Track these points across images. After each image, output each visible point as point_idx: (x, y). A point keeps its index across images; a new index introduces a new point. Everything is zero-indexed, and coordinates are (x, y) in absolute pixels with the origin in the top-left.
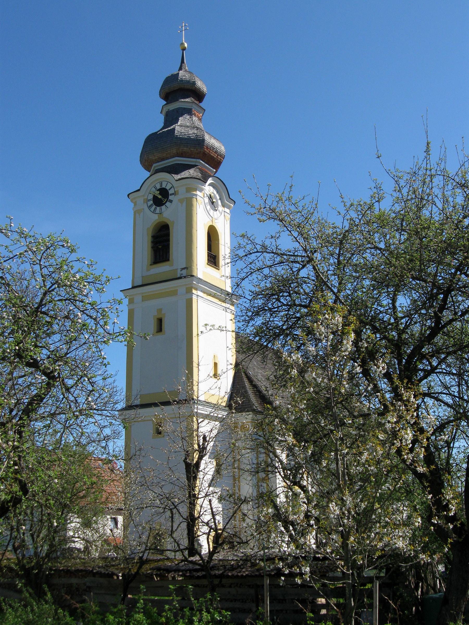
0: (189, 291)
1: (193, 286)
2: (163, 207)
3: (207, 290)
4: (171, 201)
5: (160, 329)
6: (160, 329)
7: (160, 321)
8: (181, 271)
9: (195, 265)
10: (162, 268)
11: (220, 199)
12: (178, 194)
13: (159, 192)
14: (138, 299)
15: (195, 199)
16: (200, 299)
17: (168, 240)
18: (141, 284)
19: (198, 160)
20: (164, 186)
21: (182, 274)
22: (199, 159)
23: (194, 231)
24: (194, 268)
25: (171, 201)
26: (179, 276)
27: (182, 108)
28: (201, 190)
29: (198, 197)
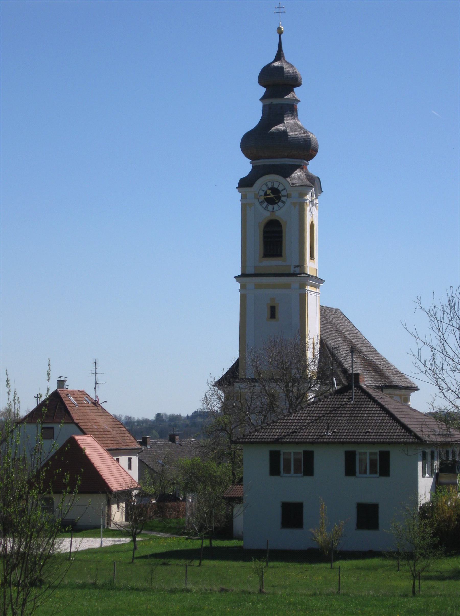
0: (302, 287)
2: (276, 206)
8: (294, 268)
15: (306, 203)
17: (281, 237)
18: (253, 272)
20: (276, 186)
21: (295, 271)
25: (284, 202)
26: (292, 272)
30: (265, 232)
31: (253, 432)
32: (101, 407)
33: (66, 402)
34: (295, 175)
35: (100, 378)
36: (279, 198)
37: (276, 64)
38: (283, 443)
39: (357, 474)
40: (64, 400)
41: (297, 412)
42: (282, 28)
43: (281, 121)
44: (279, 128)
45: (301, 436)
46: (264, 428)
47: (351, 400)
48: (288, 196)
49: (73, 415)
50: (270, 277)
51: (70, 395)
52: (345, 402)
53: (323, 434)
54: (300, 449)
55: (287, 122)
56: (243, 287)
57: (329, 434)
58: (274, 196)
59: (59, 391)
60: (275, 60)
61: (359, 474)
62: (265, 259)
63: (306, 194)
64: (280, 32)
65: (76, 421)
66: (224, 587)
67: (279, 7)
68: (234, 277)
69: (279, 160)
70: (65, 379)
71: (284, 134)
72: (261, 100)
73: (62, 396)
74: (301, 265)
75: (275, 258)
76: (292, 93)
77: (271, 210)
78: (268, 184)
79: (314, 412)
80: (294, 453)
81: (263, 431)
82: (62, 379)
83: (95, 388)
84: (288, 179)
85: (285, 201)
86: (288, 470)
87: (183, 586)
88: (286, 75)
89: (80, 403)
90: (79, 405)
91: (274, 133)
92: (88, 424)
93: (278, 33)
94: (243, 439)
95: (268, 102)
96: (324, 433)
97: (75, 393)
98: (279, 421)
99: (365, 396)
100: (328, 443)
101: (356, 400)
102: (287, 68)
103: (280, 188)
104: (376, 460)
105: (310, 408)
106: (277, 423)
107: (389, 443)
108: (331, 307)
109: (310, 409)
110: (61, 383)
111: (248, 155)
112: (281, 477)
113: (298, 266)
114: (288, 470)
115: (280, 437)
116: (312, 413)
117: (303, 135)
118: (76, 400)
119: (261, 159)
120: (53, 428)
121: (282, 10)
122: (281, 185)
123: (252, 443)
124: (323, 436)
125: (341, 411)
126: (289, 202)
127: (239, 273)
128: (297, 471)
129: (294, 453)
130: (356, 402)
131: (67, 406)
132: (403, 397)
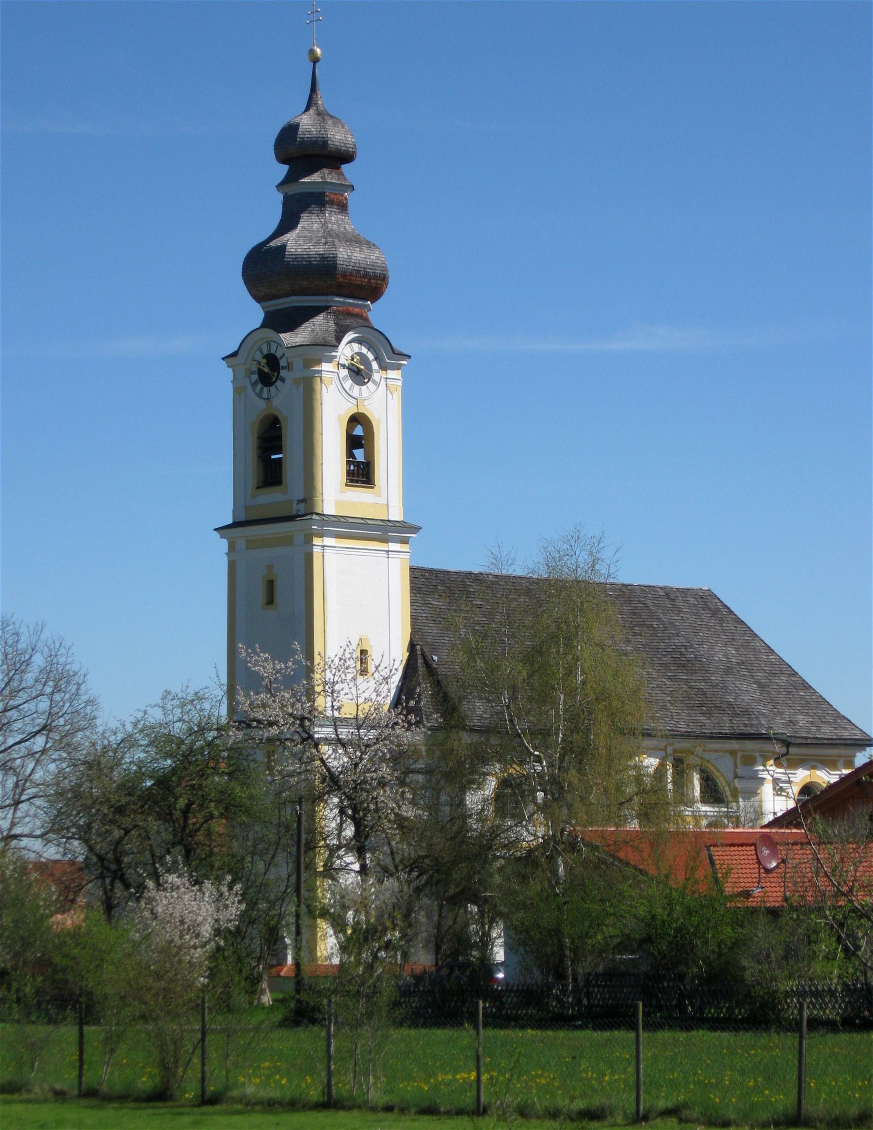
0: (308, 542)
1: (314, 532)
2: (273, 388)
5: (270, 601)
6: (270, 601)
7: (271, 585)
9: (319, 495)
10: (272, 497)
11: (376, 359)
12: (292, 370)
14: (241, 544)
15: (319, 379)
16: (328, 552)
19: (329, 298)
23: (317, 434)
24: (318, 499)
27: (305, 193)
28: (330, 360)
29: (324, 375)
48: (288, 367)
50: (255, 525)
68: (215, 530)
72: (280, 186)
88: (300, 138)
108: (652, 584)
132: (739, 754)
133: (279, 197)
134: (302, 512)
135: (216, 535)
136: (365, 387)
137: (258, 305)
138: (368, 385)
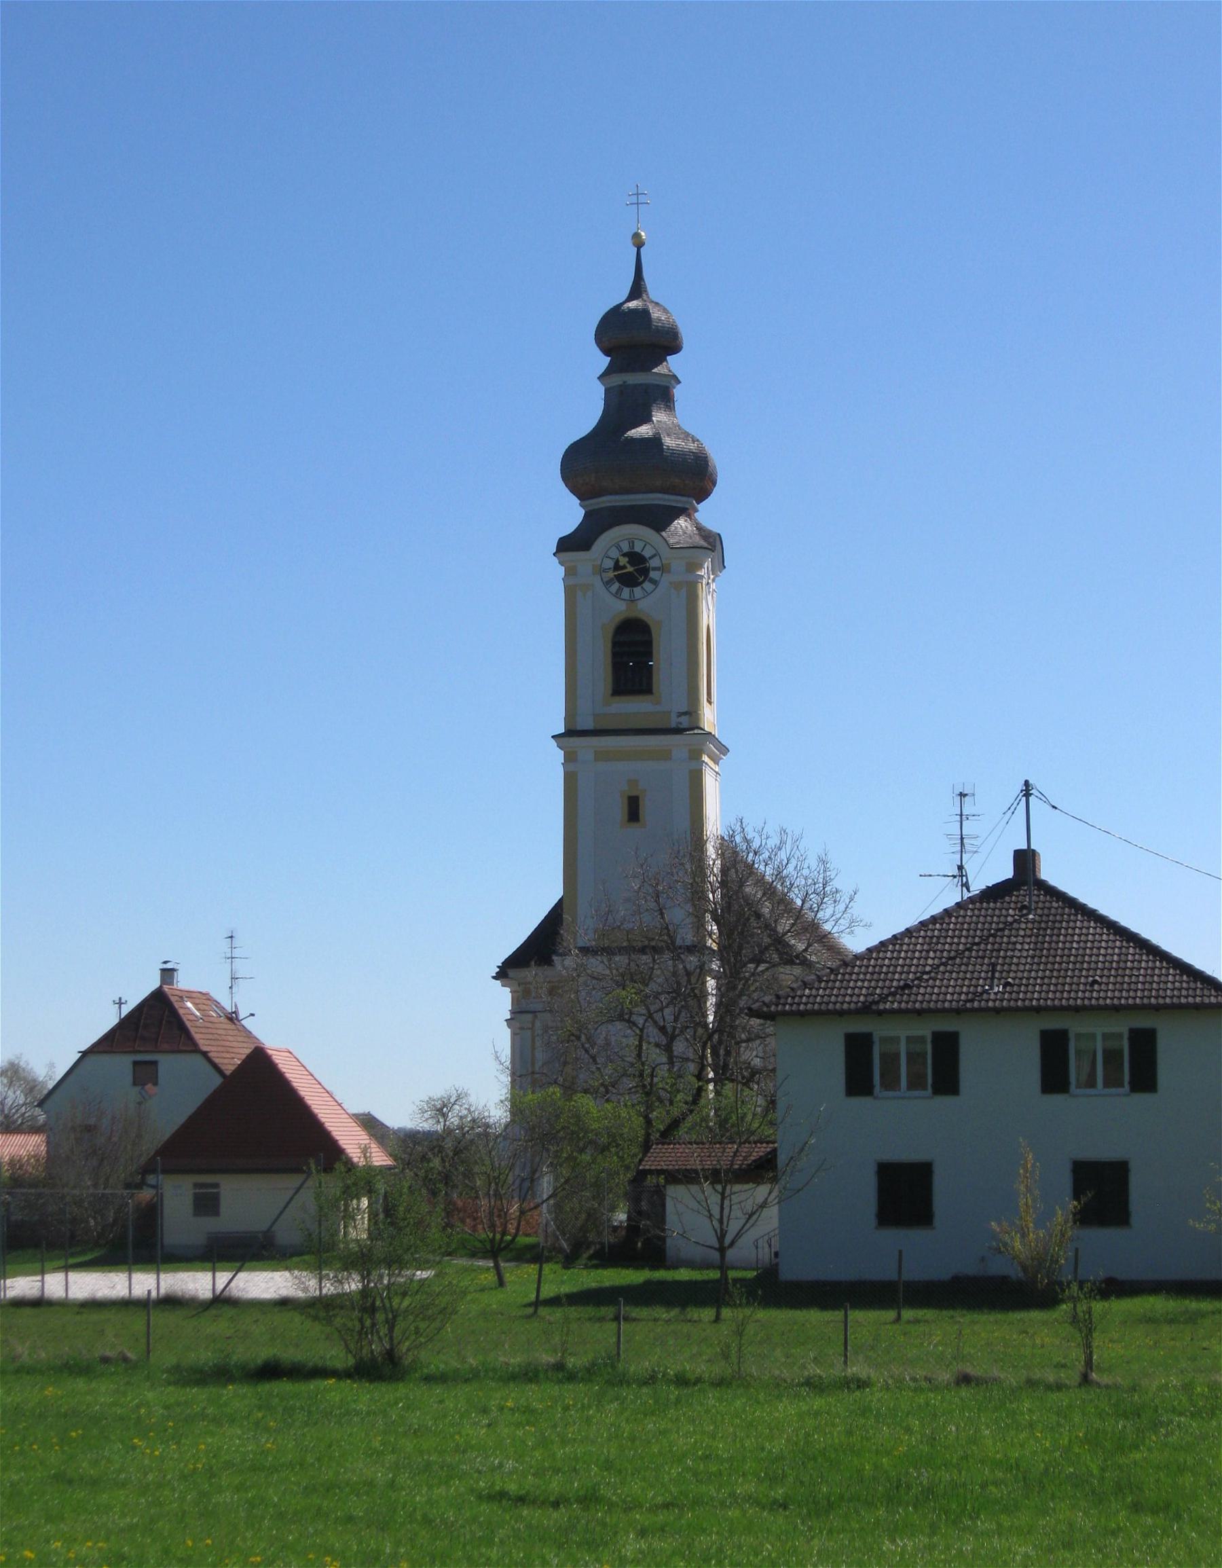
0: (695, 755)
2: (637, 590)
3: (714, 752)
4: (655, 582)
8: (678, 716)
10: (633, 707)
13: (627, 559)
20: (637, 549)
21: (681, 723)
22: (689, 496)
25: (655, 582)
26: (673, 725)
30: (615, 644)
31: (799, 988)
32: (243, 1026)
33: (181, 1012)
34: (676, 528)
35: (242, 968)
36: (645, 572)
37: (633, 304)
38: (880, 1013)
39: (1073, 1087)
40: (177, 1007)
41: (899, 942)
42: (643, 234)
43: (647, 419)
44: (644, 431)
45: (922, 997)
46: (825, 979)
47: (1025, 912)
48: (663, 569)
49: (197, 1037)
51: (186, 999)
52: (1013, 916)
53: (979, 989)
54: (925, 1030)
55: (657, 421)
56: (570, 758)
57: (996, 989)
58: (635, 570)
59: (166, 990)
60: (630, 299)
61: (1076, 1088)
62: (617, 698)
63: (701, 567)
64: (639, 244)
65: (205, 1049)
66: (970, 1370)
67: (635, 192)
69: (640, 496)
70: (175, 967)
71: (654, 442)
73: (173, 999)
74: (692, 712)
75: (631, 698)
76: (665, 363)
77: (628, 598)
78: (622, 545)
79: (942, 941)
80: (908, 1038)
81: (823, 985)
82: (169, 966)
83: (231, 988)
84: (664, 534)
85: (657, 579)
86: (890, 1082)
87: (837, 1372)
89: (205, 1015)
90: (204, 1018)
91: (633, 440)
92: (224, 1055)
93: (634, 245)
94: (777, 1005)
95: (617, 380)
96: (983, 986)
97: (194, 995)
98: (858, 963)
99: (1057, 902)
100: (997, 1011)
101: (1039, 912)
102: (656, 314)
103: (647, 553)
104: (1121, 1052)
105: (929, 932)
106: (853, 967)
107: (1157, 1008)
109: (929, 933)
110: (168, 974)
111: (575, 490)
112: (876, 1098)
113: (685, 713)
114: (890, 1082)
115: (870, 999)
116: (937, 943)
117: (692, 446)
118: (198, 1010)
119: (603, 495)
120: (154, 1063)
121: (642, 199)
122: (648, 546)
123: (802, 1014)
124: (981, 994)
125: (1009, 937)
126: (665, 580)
127: (561, 729)
128: (916, 1082)
129: (908, 1038)
130: (1040, 916)
131: (185, 1019)
133: (599, 391)
134: (685, 725)
135: (553, 743)
136: (639, 588)
137: (576, 501)
138: (644, 585)
